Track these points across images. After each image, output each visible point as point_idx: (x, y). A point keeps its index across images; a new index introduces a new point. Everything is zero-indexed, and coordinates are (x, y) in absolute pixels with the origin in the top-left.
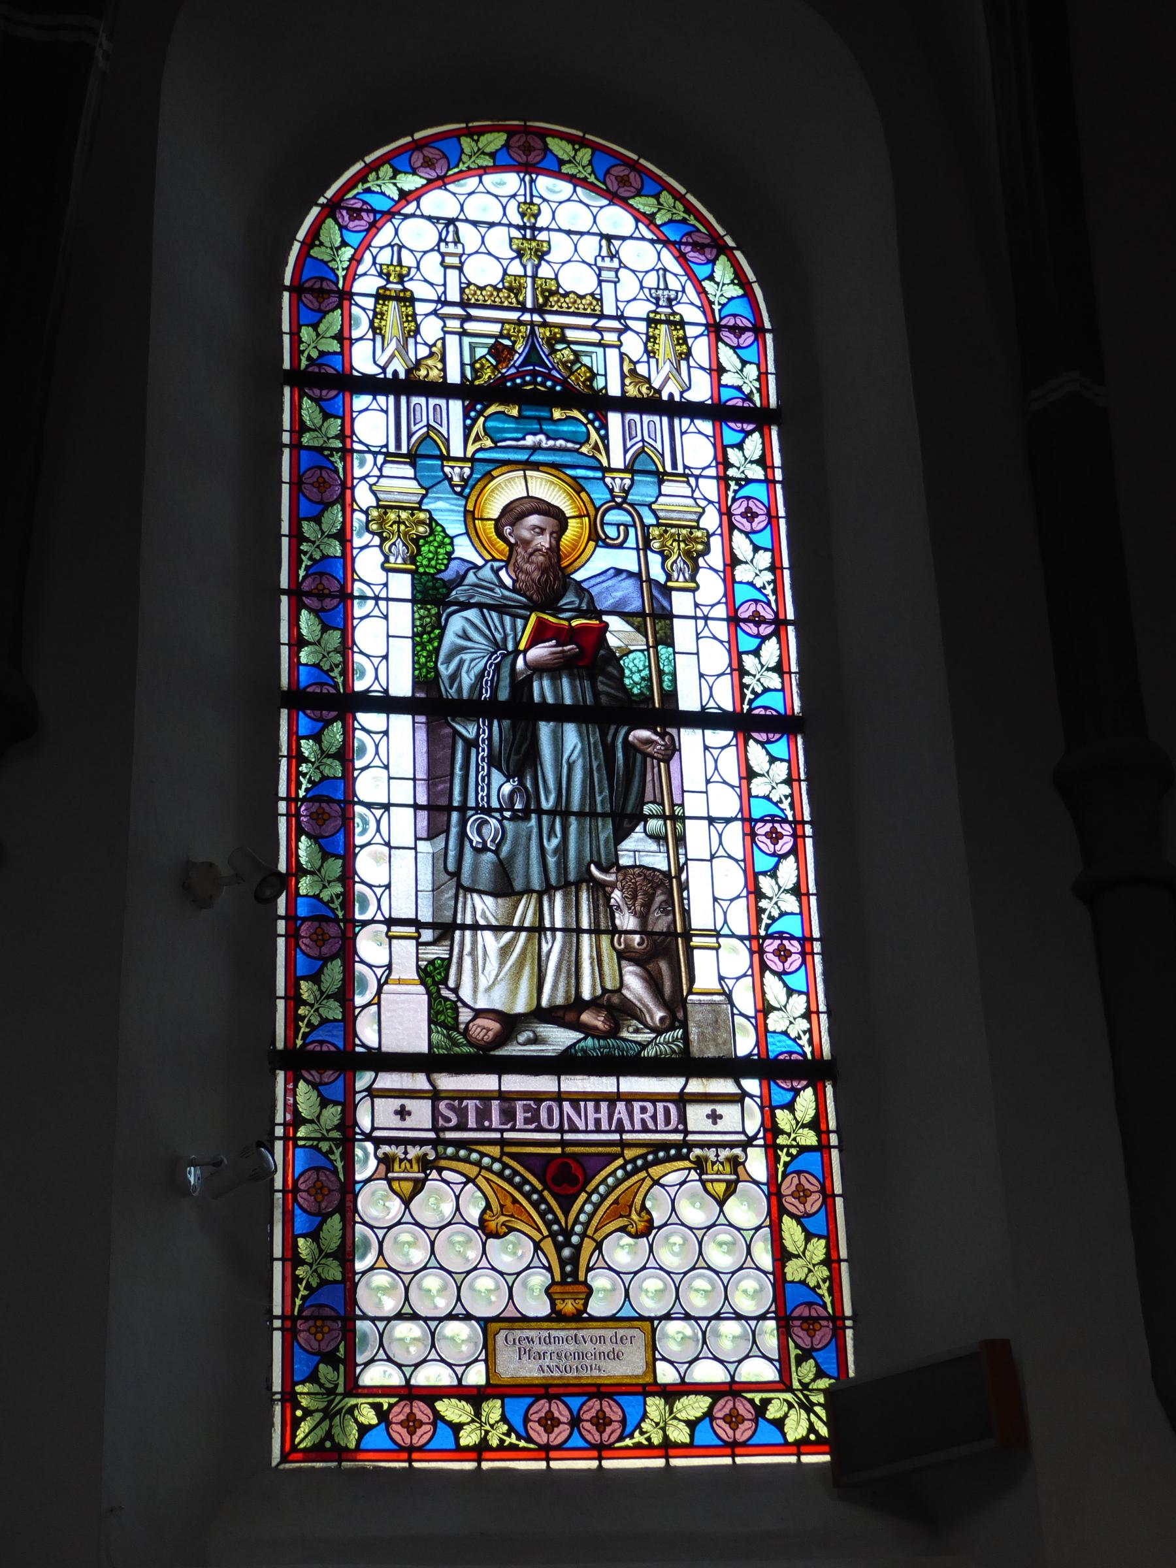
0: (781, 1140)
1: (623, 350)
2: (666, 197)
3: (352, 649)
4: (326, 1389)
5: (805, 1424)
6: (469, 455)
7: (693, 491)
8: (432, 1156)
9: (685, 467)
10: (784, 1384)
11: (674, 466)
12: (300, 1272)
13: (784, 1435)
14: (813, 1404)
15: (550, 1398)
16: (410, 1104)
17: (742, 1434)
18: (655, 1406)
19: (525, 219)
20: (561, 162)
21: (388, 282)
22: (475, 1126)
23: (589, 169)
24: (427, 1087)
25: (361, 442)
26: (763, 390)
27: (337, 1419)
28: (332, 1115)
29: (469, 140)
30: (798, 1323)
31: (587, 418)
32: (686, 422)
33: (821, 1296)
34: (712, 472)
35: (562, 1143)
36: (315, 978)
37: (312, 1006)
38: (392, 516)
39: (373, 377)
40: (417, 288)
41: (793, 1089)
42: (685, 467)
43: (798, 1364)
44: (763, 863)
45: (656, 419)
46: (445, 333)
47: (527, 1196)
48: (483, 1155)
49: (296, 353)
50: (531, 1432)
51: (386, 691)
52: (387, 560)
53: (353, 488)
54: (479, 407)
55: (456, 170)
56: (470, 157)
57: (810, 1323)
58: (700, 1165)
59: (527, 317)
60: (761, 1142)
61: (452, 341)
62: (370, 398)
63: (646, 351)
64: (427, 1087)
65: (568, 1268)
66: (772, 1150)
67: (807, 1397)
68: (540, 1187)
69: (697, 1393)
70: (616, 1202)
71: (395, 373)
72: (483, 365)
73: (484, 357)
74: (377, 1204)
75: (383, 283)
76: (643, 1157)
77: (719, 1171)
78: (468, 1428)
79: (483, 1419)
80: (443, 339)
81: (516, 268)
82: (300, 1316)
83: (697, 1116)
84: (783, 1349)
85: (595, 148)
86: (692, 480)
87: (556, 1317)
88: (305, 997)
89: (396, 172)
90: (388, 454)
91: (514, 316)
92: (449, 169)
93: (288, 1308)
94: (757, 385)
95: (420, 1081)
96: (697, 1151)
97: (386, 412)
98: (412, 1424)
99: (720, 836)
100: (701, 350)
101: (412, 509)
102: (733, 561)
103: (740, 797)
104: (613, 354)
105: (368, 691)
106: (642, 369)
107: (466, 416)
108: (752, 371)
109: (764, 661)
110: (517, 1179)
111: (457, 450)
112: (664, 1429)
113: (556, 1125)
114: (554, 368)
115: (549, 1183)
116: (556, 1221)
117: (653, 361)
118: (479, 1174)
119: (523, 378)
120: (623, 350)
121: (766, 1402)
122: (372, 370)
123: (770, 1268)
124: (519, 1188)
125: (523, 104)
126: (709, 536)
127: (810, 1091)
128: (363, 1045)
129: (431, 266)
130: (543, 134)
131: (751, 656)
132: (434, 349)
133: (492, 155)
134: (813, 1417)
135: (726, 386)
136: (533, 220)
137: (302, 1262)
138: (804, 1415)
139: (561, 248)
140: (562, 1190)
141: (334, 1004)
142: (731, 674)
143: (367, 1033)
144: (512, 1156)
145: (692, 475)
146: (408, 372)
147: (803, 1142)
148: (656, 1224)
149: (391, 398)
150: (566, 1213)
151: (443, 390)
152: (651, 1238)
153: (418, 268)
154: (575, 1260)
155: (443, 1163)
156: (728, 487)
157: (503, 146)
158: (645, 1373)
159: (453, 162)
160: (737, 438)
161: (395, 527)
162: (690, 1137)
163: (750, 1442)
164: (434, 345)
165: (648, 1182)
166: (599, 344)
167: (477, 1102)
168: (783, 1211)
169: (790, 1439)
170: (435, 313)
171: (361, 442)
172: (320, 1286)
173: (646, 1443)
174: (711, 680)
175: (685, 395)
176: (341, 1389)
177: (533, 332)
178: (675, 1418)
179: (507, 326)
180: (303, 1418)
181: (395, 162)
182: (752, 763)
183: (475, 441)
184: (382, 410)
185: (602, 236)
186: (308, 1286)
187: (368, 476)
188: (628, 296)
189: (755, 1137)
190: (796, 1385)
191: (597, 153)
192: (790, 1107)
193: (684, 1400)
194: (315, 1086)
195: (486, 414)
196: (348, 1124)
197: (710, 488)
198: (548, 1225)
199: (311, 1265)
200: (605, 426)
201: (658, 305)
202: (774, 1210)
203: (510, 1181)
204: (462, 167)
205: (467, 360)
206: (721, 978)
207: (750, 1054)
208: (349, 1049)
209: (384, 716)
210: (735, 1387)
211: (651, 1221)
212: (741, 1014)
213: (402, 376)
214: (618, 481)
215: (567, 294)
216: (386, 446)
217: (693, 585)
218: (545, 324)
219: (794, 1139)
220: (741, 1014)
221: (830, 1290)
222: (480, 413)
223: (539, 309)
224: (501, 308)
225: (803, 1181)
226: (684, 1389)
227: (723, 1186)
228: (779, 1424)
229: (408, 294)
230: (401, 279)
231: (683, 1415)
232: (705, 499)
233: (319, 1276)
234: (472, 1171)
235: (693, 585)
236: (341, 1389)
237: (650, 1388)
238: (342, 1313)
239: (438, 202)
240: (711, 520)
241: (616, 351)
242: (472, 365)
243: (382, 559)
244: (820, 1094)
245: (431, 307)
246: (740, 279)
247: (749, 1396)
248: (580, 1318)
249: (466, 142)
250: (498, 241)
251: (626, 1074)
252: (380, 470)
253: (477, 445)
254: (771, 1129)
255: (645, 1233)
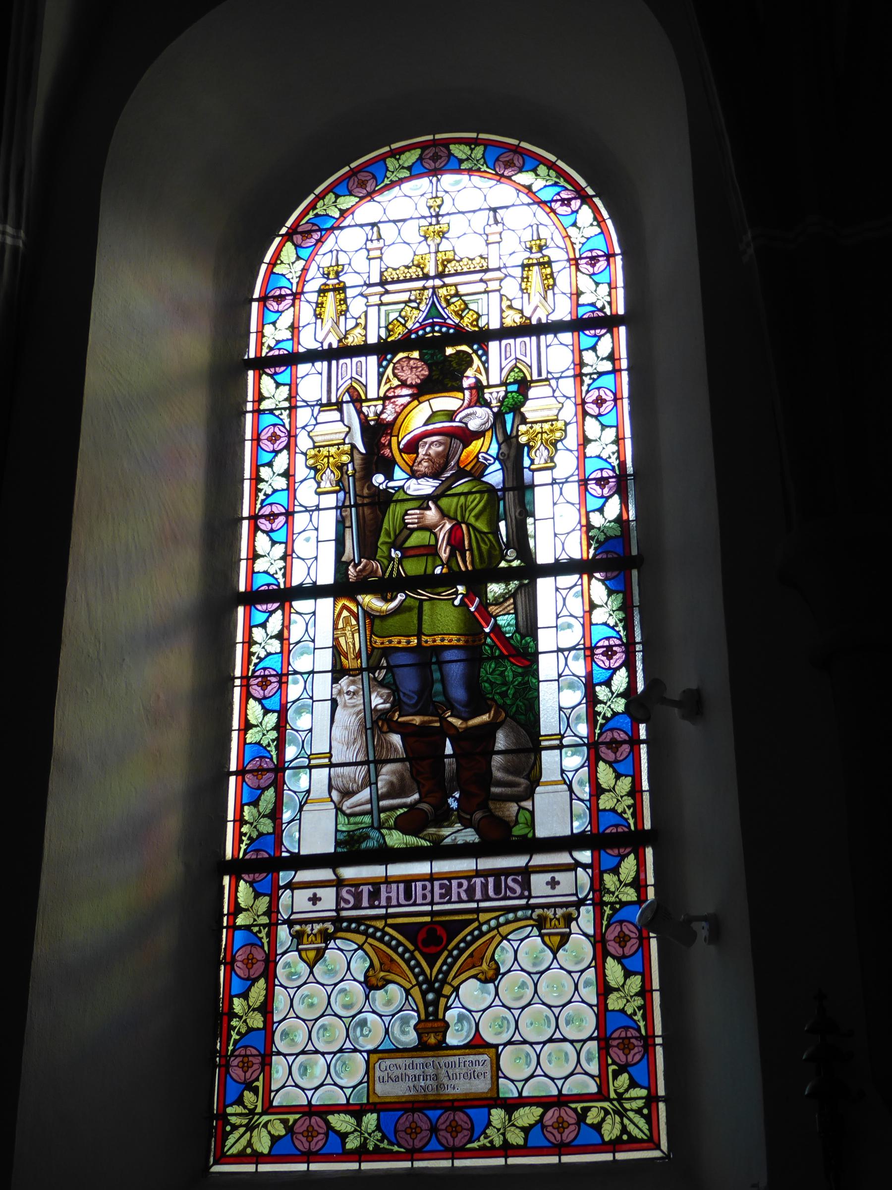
0: (606, 898)
1: (502, 292)
2: (542, 170)
3: (291, 555)
4: (248, 1109)
5: (618, 1127)
6: (381, 395)
7: (554, 391)
8: (331, 929)
9: (548, 372)
10: (602, 1095)
11: (540, 374)
12: (245, 829)
13: (602, 1136)
14: (626, 1110)
15: (413, 1111)
16: (320, 892)
17: (568, 1135)
18: (497, 1115)
19: (432, 210)
20: (461, 161)
21: (328, 279)
22: (367, 905)
23: (482, 161)
24: (334, 877)
25: (301, 505)
26: (637, 813)
27: (255, 1132)
28: (263, 903)
29: (393, 159)
30: (584, 261)
31: (472, 349)
32: (550, 337)
33: (626, 820)
34: (571, 373)
35: (432, 914)
36: (255, 803)
37: (251, 824)
38: (324, 451)
39: (316, 350)
40: (348, 279)
41: (619, 855)
42: (548, 372)
43: (615, 1078)
44: (599, 675)
45: (527, 339)
46: (368, 306)
47: (401, 956)
48: (369, 927)
49: (260, 344)
50: (399, 1140)
51: (315, 583)
52: (319, 487)
53: (296, 436)
54: (389, 357)
55: (382, 185)
56: (393, 172)
57: (626, 1045)
58: (540, 924)
59: (430, 283)
60: (582, 646)
61: (373, 311)
62: (310, 365)
63: (522, 290)
64: (334, 877)
65: (431, 1009)
66: (598, 905)
67: (621, 1105)
68: (411, 948)
69: (531, 1105)
70: (471, 955)
71: (330, 345)
72: (394, 325)
73: (396, 319)
74: (290, 965)
75: (324, 280)
76: (497, 918)
77: (553, 925)
78: (351, 1137)
79: (363, 1128)
80: (366, 312)
81: (423, 249)
82: (252, 676)
83: (539, 882)
84: (603, 1066)
85: (487, 144)
86: (553, 382)
87: (422, 1048)
88: (246, 818)
89: (337, 196)
90: (322, 405)
91: (420, 284)
92: (377, 186)
93: (252, 510)
94: (608, 299)
95: (326, 874)
96: (538, 911)
97: (321, 374)
98: (310, 1133)
99: (564, 599)
100: (564, 281)
101: (338, 444)
102: (585, 441)
103: (583, 625)
104: (495, 296)
105: (302, 584)
106: (517, 304)
107: (380, 365)
108: (604, 289)
109: (599, 354)
110: (394, 943)
111: (372, 393)
112: (504, 1134)
113: (429, 900)
114: (449, 317)
115: (420, 944)
116: (423, 972)
117: (526, 296)
118: (366, 941)
119: (424, 329)
120: (502, 292)
121: (586, 1110)
122: (315, 346)
123: (595, 1002)
124: (395, 950)
125: (433, 122)
126: (566, 424)
127: (632, 856)
128: (288, 851)
129: (360, 262)
130: (446, 143)
131: (590, 351)
132: (359, 321)
133: (409, 168)
134: (626, 1121)
135: (583, 305)
136: (437, 210)
137: (246, 822)
138: (618, 1119)
139: (457, 225)
140: (432, 951)
141: (267, 821)
142: (580, 530)
143: (290, 845)
144: (392, 926)
145: (554, 378)
146: (340, 341)
147: (624, 898)
148: (502, 971)
149: (325, 363)
150: (431, 968)
151: (364, 350)
152: (496, 983)
153: (350, 264)
154: (435, 1003)
155: (339, 934)
156: (582, 382)
157: (418, 159)
158: (491, 1090)
159: (379, 181)
160: (591, 341)
161: (326, 460)
162: (532, 901)
163: (573, 1143)
164: (360, 317)
165: (498, 938)
166: (486, 292)
167: (370, 887)
168: (606, 954)
169: (607, 1139)
170: (361, 295)
171: (301, 505)
172: (247, 1032)
173: (488, 1145)
174: (563, 538)
175: (550, 317)
176: (259, 1110)
177: (434, 293)
178: (513, 1125)
179: (413, 292)
180: (231, 1132)
181: (336, 190)
182: (587, 433)
183: (386, 383)
184: (319, 373)
185: (490, 209)
186: (250, 838)
187: (306, 425)
188: (511, 251)
189: (585, 899)
190: (613, 1095)
191: (489, 148)
192: (615, 871)
193: (522, 1111)
194: (251, 883)
195: (395, 361)
196: (272, 910)
197: (568, 386)
198: (416, 976)
199: (251, 824)
200: (486, 353)
201: (531, 253)
202: (592, 757)
203: (388, 945)
204: (387, 181)
205: (383, 324)
206: (563, 771)
207: (584, 831)
208: (277, 855)
209: (313, 601)
210: (562, 1099)
211: (498, 968)
212: (579, 799)
213: (335, 346)
214: (495, 395)
215: (461, 260)
216: (321, 400)
217: (552, 464)
218: (445, 285)
219: (617, 896)
220: (579, 799)
221: (634, 815)
222: (390, 361)
223: (441, 275)
224: (411, 280)
225: (625, 929)
226: (522, 1102)
227: (558, 938)
228: (597, 1127)
229: (342, 284)
230: (337, 275)
231: (520, 1123)
232: (564, 396)
233: (258, 830)
234: (360, 939)
235: (552, 464)
236: (259, 1110)
237: (494, 1100)
238: (262, 1052)
239: (368, 211)
240: (569, 412)
241: (498, 293)
242: (387, 327)
243: (316, 486)
244: (641, 857)
245: (357, 291)
246: (598, 220)
247: (573, 1106)
248: (441, 1046)
249: (391, 163)
250: (411, 231)
251: (480, 857)
252: (316, 419)
253: (388, 386)
254: (597, 886)
255: (492, 980)
